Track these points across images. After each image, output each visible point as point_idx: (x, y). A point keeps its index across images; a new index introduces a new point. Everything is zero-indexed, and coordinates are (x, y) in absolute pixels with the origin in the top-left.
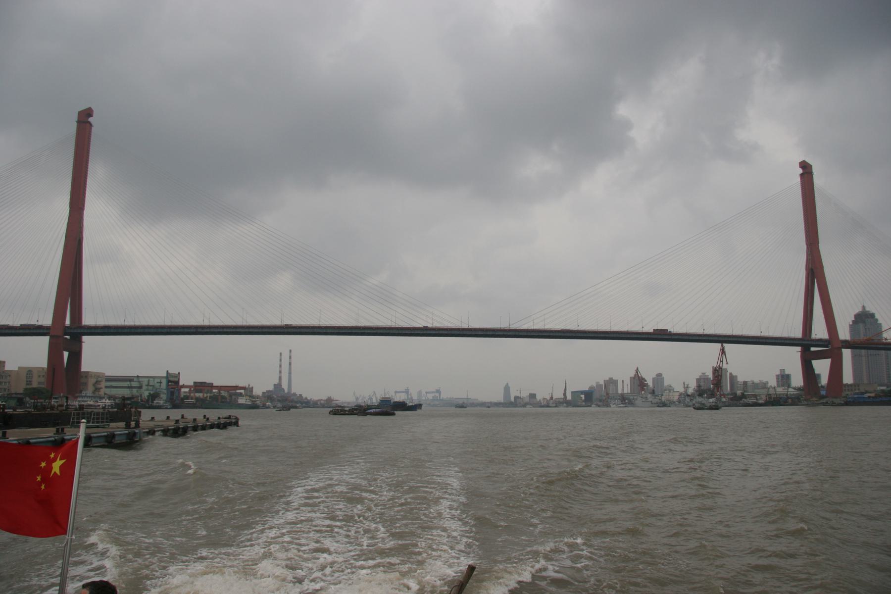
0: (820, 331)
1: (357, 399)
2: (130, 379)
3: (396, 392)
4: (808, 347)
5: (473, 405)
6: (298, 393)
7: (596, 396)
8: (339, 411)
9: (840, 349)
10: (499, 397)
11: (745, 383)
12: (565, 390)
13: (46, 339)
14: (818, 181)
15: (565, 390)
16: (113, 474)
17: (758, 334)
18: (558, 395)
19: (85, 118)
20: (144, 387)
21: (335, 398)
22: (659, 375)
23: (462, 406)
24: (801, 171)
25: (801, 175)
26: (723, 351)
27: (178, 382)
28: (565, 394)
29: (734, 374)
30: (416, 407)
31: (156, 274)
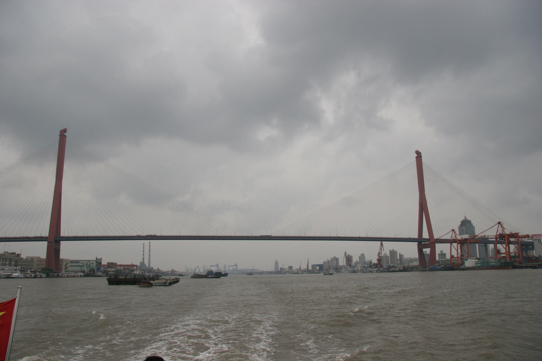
0: (426, 235)
1: (187, 270)
2: (77, 262)
3: (211, 266)
4: (421, 243)
5: (256, 273)
6: (155, 268)
7: (325, 267)
8: (197, 276)
9: (434, 244)
10: (272, 268)
11: (401, 256)
12: (308, 264)
13: (46, 243)
15: (308, 264)
17: (394, 237)
18: (304, 267)
19: (63, 134)
20: (85, 266)
21: (177, 270)
22: (363, 255)
23: (251, 274)
24: (416, 155)
25: (416, 157)
26: (382, 245)
27: (101, 263)
28: (308, 266)
29: (402, 254)
30: (226, 275)
31: (102, 209)
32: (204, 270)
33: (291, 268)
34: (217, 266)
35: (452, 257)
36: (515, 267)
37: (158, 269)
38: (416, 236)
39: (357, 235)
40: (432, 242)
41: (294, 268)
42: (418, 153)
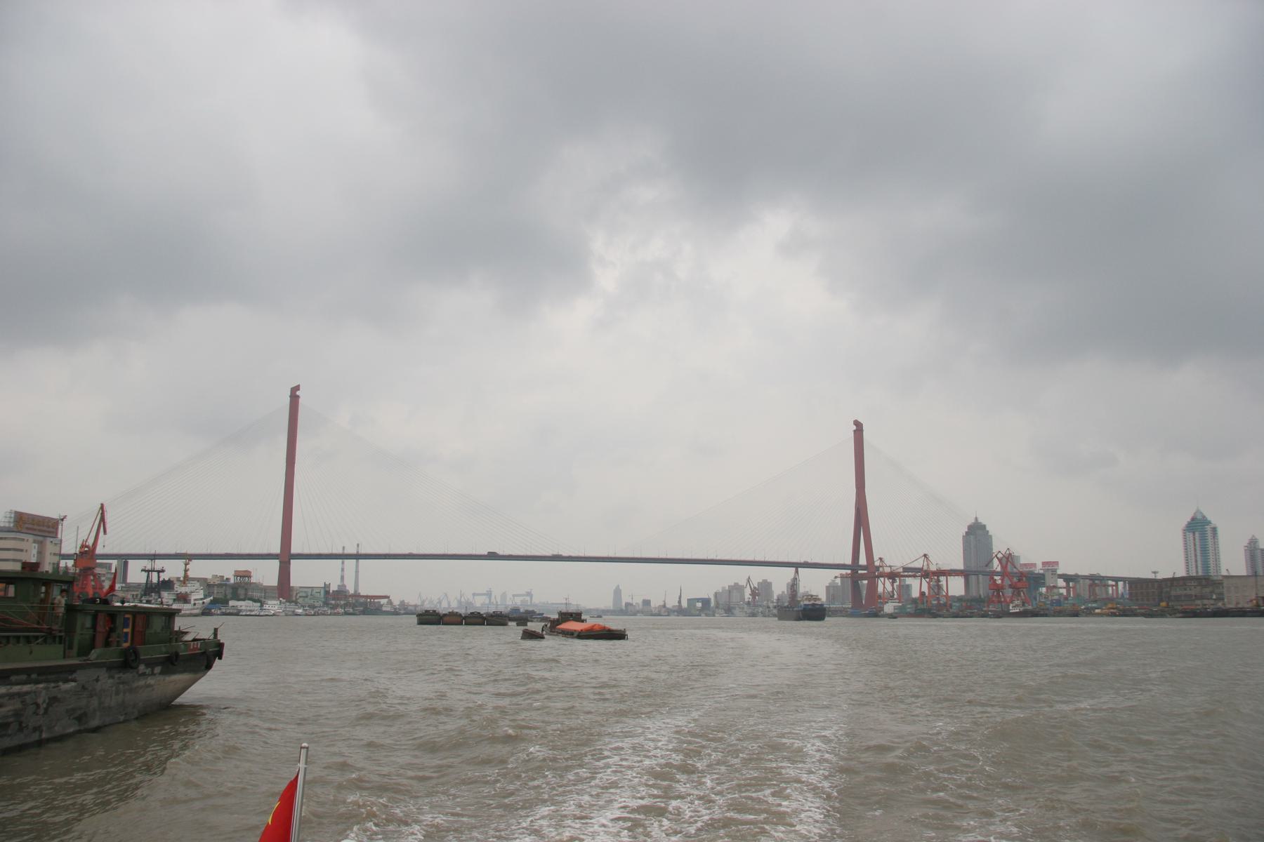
0: (863, 560)
3: (474, 594)
11: (1008, 559)
14: (302, 402)
16: (420, 769)
18: (672, 603)
26: (797, 572)
32: (460, 602)
33: (647, 603)
34: (489, 594)
35: (922, 594)
36: (935, 616)
37: (402, 603)
38: (849, 561)
39: (750, 558)
40: (874, 572)
41: (653, 605)
42: (859, 427)
